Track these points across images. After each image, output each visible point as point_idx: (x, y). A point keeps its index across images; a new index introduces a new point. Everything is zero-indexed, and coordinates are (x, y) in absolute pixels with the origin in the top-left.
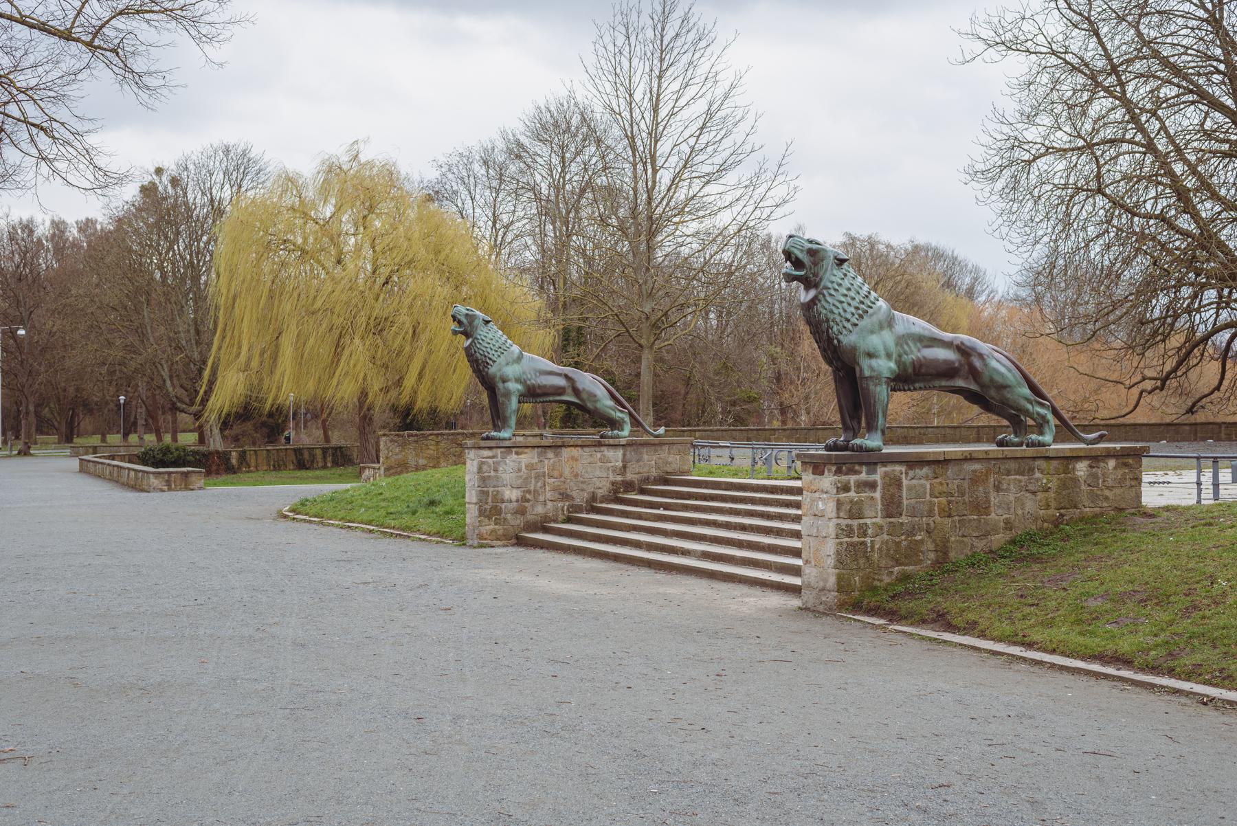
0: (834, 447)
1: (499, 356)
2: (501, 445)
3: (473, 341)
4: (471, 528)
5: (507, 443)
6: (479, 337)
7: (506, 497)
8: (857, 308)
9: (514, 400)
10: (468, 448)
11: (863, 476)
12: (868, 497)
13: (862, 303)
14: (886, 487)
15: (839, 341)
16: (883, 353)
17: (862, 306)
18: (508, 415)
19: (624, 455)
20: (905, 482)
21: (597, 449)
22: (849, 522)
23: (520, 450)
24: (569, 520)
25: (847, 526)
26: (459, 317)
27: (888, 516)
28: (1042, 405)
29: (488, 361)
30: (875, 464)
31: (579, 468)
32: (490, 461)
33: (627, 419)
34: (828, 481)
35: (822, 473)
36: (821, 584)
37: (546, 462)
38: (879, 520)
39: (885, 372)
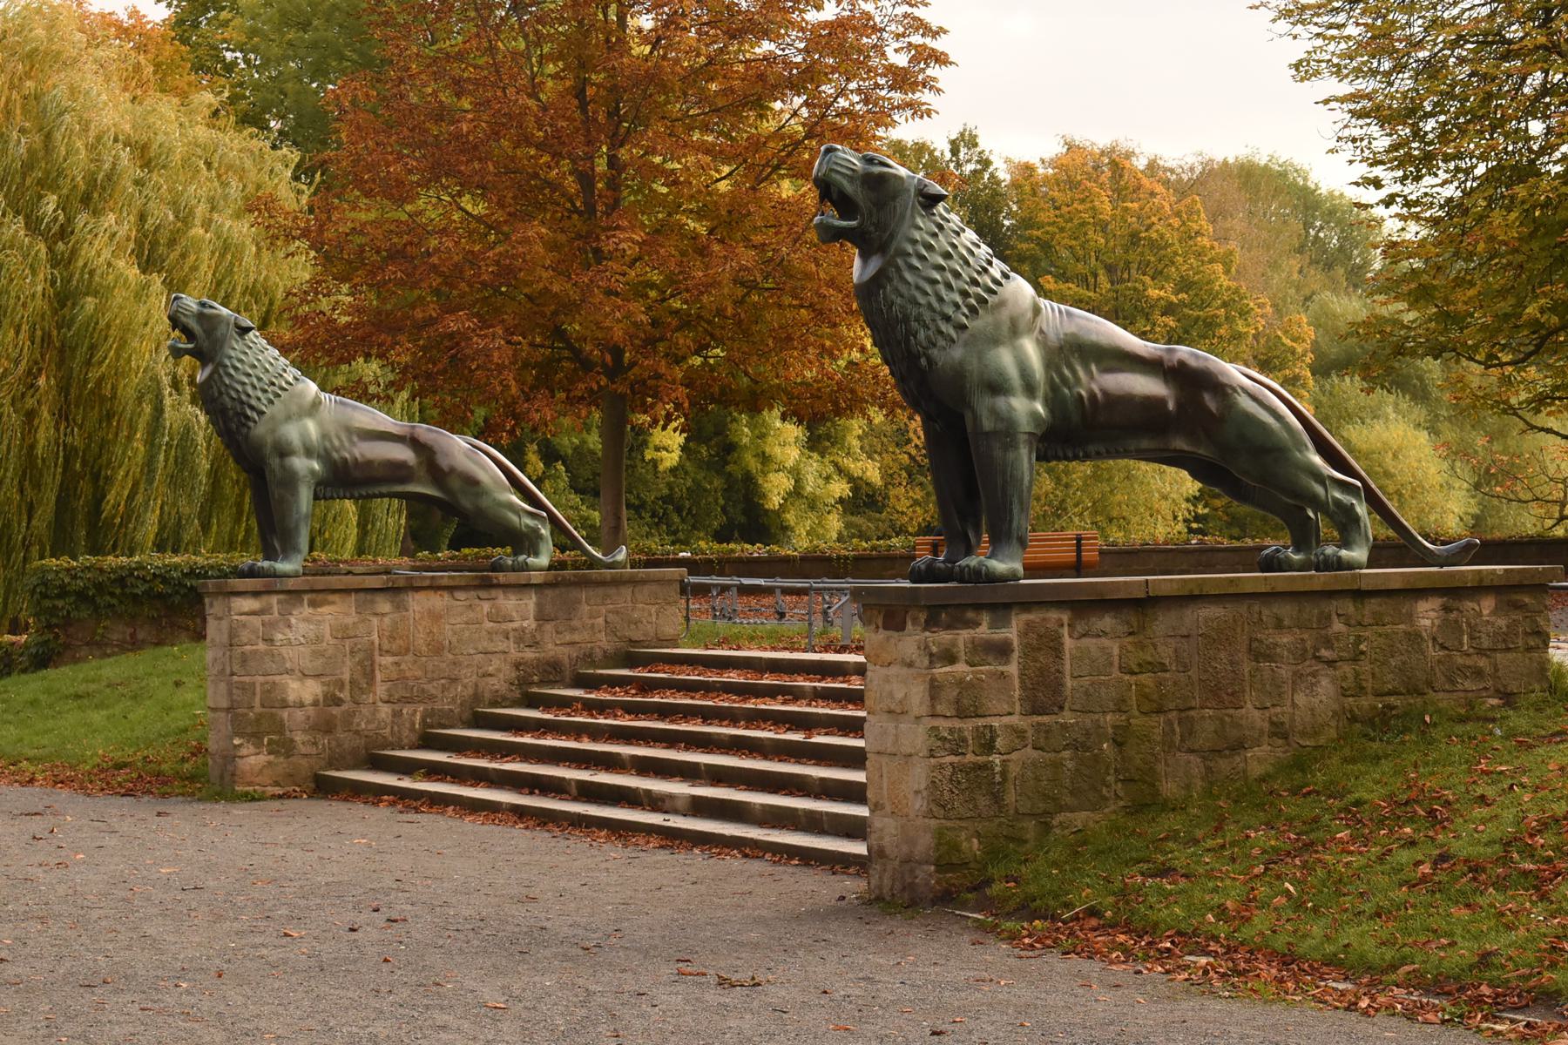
1: (271, 402)
2: (279, 587)
4: (220, 761)
5: (291, 584)
6: (227, 362)
7: (291, 698)
8: (965, 294)
9: (305, 495)
10: (210, 594)
11: (984, 631)
12: (991, 674)
14: (1029, 651)
15: (930, 360)
17: (973, 290)
19: (539, 606)
20: (1068, 643)
21: (483, 594)
22: (957, 724)
23: (321, 596)
24: (428, 742)
25: (951, 731)
26: (184, 319)
27: (1035, 712)
29: (249, 412)
30: (1007, 607)
31: (447, 633)
32: (256, 621)
33: (545, 531)
34: (910, 642)
35: (901, 627)
36: (905, 849)
37: (375, 621)
38: (1015, 720)
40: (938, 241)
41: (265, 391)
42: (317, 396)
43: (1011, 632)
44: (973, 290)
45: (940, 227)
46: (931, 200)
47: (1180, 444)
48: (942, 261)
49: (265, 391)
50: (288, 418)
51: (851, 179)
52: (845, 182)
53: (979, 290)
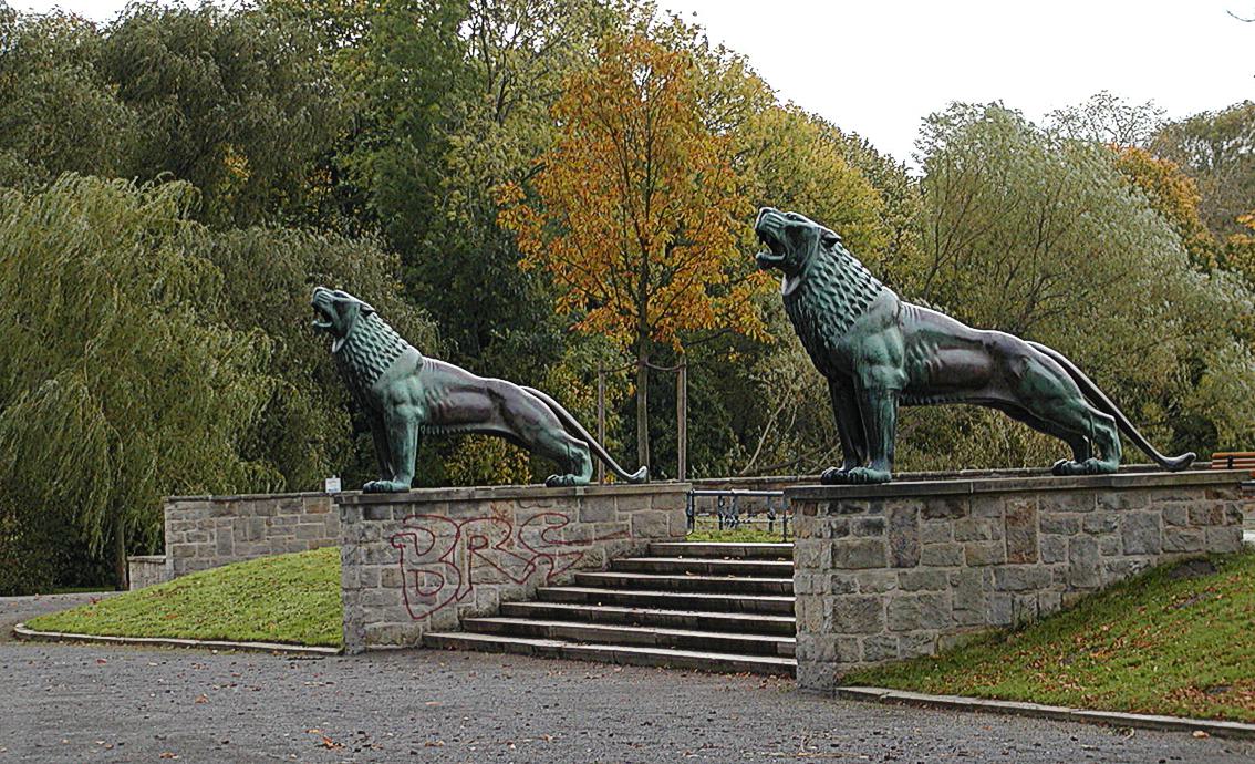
0: (834, 478)
3: (346, 343)
5: (402, 497)
6: (355, 336)
8: (852, 301)
13: (859, 294)
15: (831, 343)
16: (409, 399)
17: (857, 298)
26: (323, 306)
28: (1104, 421)
29: (371, 372)
33: (587, 457)
34: (823, 521)
39: (890, 381)
40: (834, 268)
41: (382, 357)
42: (420, 358)
43: (883, 516)
44: (857, 298)
45: (836, 260)
46: (830, 242)
47: (993, 394)
48: (837, 281)
49: (382, 357)
50: (399, 377)
51: (779, 230)
52: (775, 232)
53: (861, 298)
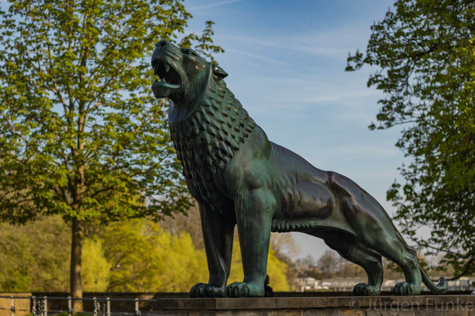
18: (259, 250)
